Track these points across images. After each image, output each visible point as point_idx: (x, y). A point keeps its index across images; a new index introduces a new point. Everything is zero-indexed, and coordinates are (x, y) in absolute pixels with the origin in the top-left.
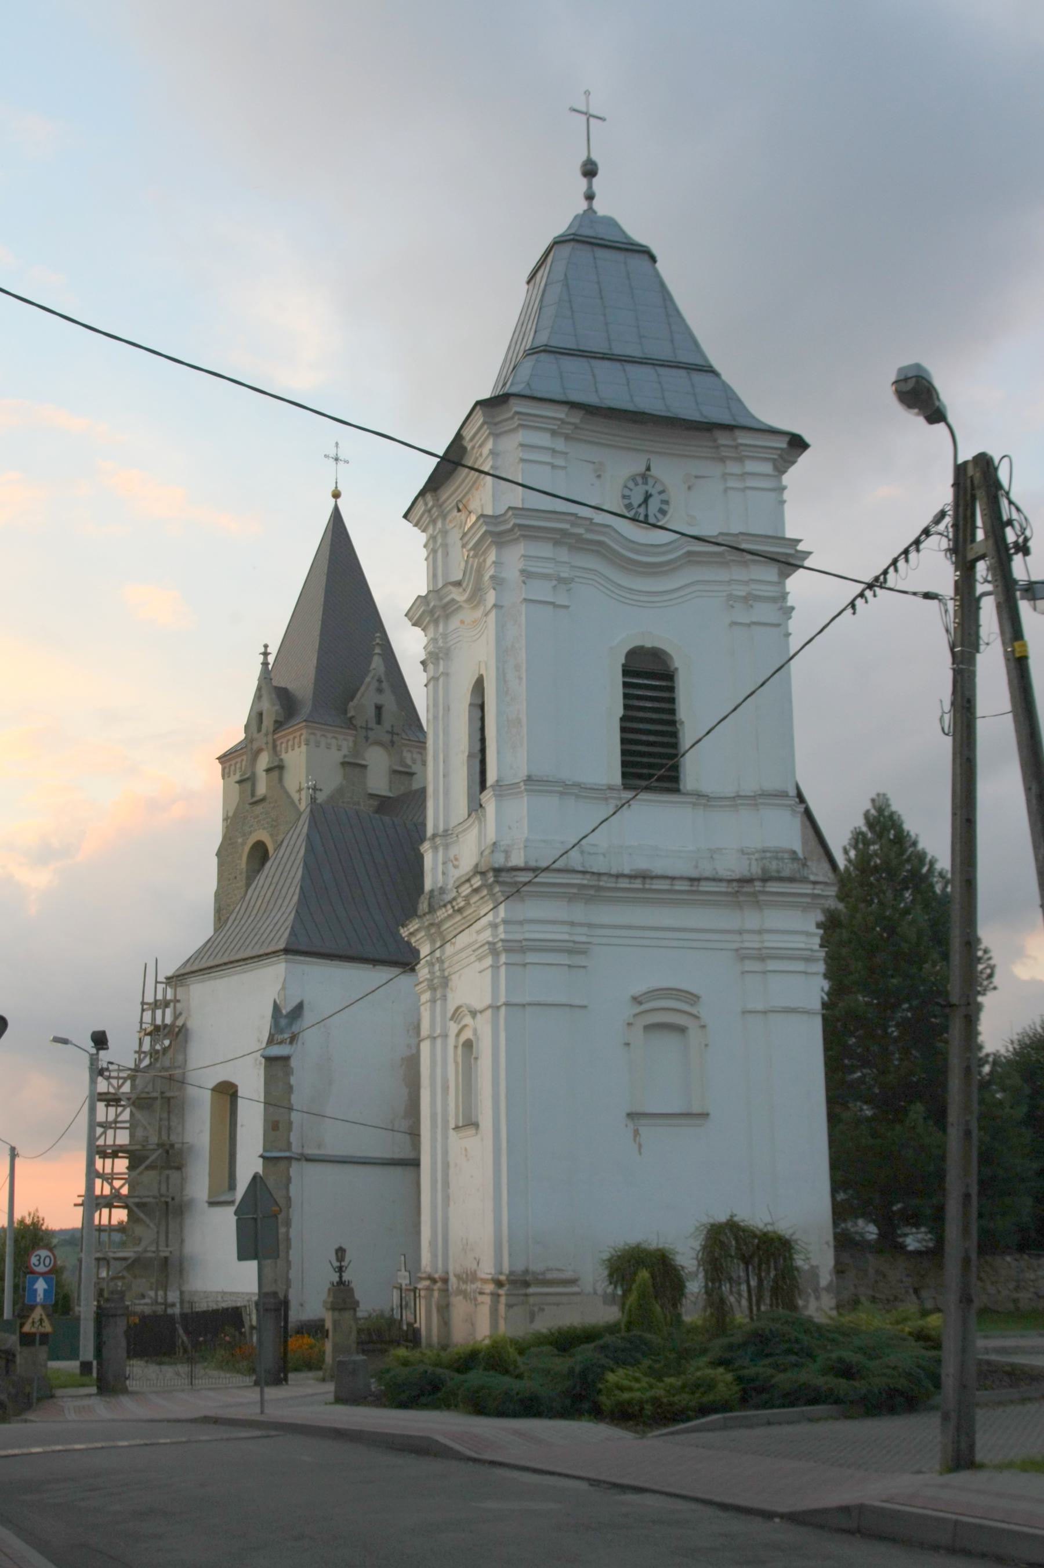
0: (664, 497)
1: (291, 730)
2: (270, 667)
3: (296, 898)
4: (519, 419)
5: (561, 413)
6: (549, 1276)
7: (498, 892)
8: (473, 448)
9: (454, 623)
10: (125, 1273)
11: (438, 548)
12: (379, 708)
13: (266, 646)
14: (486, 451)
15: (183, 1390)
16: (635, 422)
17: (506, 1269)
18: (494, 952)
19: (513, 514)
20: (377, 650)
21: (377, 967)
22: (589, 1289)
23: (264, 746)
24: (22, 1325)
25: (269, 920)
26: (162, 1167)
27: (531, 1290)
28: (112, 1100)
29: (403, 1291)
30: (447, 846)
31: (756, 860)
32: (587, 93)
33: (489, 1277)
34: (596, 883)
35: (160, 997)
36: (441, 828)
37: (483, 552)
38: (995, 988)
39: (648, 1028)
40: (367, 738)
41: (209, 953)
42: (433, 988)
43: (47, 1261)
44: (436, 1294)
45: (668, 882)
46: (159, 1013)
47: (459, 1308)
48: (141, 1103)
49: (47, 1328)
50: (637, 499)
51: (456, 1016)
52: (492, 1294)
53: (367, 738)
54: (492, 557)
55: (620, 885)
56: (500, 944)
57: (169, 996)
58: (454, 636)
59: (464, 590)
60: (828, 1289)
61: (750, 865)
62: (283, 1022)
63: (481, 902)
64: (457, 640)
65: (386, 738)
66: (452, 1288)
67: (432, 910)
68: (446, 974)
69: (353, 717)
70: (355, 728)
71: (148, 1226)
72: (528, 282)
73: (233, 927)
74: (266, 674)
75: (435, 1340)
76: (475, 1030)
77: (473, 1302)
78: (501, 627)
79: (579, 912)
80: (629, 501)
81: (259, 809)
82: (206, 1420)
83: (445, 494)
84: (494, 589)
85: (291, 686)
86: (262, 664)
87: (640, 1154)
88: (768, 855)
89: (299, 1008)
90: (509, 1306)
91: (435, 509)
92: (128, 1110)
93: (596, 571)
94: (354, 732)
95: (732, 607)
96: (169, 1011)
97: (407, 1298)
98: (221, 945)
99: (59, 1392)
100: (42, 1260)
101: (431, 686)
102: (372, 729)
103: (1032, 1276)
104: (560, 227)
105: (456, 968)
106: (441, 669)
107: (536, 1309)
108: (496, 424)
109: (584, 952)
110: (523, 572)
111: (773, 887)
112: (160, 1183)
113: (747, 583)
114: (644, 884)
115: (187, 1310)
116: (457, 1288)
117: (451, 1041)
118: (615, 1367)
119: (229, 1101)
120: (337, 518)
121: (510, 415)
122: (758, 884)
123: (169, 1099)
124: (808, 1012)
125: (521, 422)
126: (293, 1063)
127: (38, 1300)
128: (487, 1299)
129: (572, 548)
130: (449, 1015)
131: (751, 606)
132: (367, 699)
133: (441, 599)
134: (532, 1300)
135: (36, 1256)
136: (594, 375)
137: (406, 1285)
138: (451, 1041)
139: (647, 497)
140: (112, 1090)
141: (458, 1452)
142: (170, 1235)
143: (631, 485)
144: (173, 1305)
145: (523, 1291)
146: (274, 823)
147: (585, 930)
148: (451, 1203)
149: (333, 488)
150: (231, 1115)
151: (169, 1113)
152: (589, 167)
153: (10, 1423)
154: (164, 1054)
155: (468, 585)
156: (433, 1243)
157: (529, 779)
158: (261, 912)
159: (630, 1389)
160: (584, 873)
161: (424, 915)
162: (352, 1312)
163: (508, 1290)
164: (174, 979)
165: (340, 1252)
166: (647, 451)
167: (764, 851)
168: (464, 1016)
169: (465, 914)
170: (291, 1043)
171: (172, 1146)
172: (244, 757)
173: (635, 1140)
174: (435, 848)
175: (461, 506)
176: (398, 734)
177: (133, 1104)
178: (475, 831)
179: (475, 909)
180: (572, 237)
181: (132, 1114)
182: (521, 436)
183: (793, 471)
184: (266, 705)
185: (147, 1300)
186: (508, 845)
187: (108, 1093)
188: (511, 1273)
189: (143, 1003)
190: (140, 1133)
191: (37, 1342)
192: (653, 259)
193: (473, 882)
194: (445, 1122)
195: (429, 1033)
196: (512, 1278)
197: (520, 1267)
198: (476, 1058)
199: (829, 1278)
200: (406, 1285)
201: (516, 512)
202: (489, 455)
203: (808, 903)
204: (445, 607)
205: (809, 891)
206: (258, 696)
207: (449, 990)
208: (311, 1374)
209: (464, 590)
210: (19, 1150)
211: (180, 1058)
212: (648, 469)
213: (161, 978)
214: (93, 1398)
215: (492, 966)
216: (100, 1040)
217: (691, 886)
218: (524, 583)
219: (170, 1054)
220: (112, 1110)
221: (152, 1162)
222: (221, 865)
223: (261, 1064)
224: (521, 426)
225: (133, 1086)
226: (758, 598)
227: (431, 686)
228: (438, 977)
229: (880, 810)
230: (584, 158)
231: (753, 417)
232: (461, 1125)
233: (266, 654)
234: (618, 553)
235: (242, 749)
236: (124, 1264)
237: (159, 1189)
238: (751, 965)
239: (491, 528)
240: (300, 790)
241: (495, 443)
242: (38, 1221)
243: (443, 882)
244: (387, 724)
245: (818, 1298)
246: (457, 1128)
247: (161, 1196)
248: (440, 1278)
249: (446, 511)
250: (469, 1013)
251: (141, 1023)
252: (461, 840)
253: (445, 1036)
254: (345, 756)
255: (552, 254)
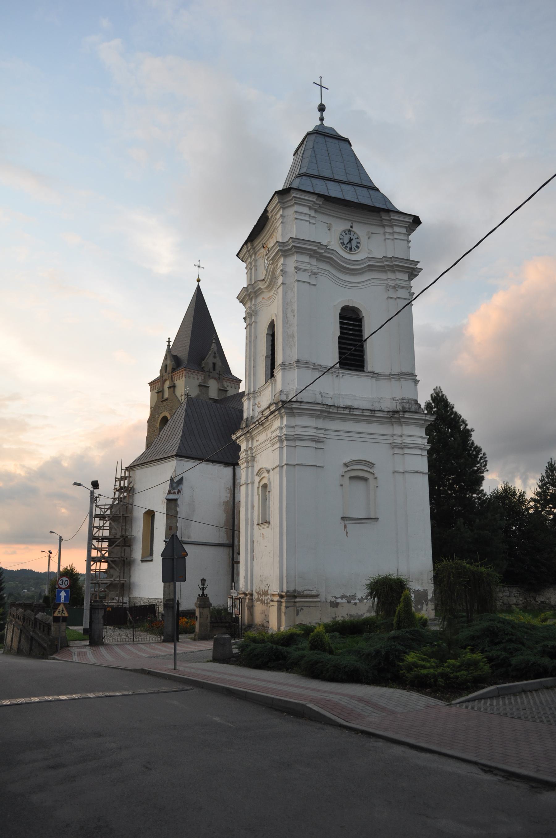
0: (358, 240)
1: (179, 371)
2: (171, 347)
3: (181, 434)
4: (295, 200)
5: (313, 198)
6: (305, 593)
7: (283, 412)
8: (272, 217)
9: (260, 299)
10: (106, 589)
11: (253, 267)
12: (214, 364)
13: (169, 339)
14: (278, 216)
15: (129, 644)
16: (346, 206)
17: (285, 589)
18: (281, 441)
19: (292, 241)
20: (214, 341)
21: (214, 464)
22: (324, 600)
23: (168, 378)
24: (54, 612)
25: (169, 443)
26: (123, 546)
27: (297, 600)
28: (101, 517)
29: (233, 600)
30: (255, 398)
31: (399, 403)
32: (321, 77)
33: (277, 593)
34: (328, 410)
35: (123, 475)
36: (252, 390)
37: (276, 262)
38: (487, 471)
39: (351, 478)
40: (209, 376)
41: (144, 458)
42: (247, 462)
43: (66, 583)
44: (247, 601)
45: (361, 411)
46: (122, 482)
47: (259, 608)
48: (114, 519)
49: (66, 614)
50: (346, 240)
51: (259, 473)
52: (278, 601)
53: (209, 376)
54: (281, 261)
55: (339, 412)
56: (284, 436)
57: (127, 475)
58: (259, 305)
59: (266, 282)
60: (431, 600)
61: (397, 405)
62: (175, 485)
63: (274, 418)
64: (261, 307)
65: (217, 376)
66: (255, 598)
67: (247, 426)
68: (254, 455)
69: (204, 367)
70: (204, 371)
71: (116, 570)
72: (294, 155)
73: (155, 446)
74: (169, 350)
75: (246, 621)
76: (269, 479)
77: (266, 605)
78: (285, 293)
79: (320, 423)
80: (343, 241)
81: (165, 403)
82: (143, 671)
83: (256, 243)
84: (282, 276)
85: (179, 355)
86: (167, 346)
87: (347, 536)
88: (405, 401)
89: (181, 480)
90: (287, 607)
91: (251, 250)
92: (108, 522)
93: (328, 271)
94: (204, 373)
95: (389, 290)
96: (126, 481)
97: (236, 603)
98: (149, 454)
99: (71, 643)
100: (64, 582)
101: (248, 328)
102: (211, 372)
103: (501, 596)
104: (311, 129)
105: (259, 451)
106: (253, 320)
107: (299, 609)
108: (283, 203)
109: (322, 442)
110: (296, 267)
111: (407, 415)
112: (121, 552)
113: (395, 280)
114: (350, 411)
115: (132, 605)
116: (258, 598)
117: (256, 485)
118: (407, 651)
119: (151, 518)
120: (198, 290)
121: (290, 198)
122: (401, 414)
123: (126, 517)
124: (423, 473)
125: (295, 201)
126: (179, 502)
127: (62, 601)
128: (276, 604)
129: (318, 260)
130: (255, 473)
131: (397, 290)
132: (209, 360)
133: (254, 289)
134: (297, 604)
135: (61, 580)
136: (327, 187)
137: (235, 596)
138: (256, 485)
139: (351, 240)
140: (102, 513)
141: (330, 719)
142: (125, 574)
143: (344, 234)
144: (126, 603)
145: (293, 600)
146: (171, 409)
147: (323, 432)
148: (255, 559)
149: (197, 278)
150: (151, 527)
151: (126, 523)
152: (322, 107)
153: (47, 659)
154: (124, 499)
155: (267, 280)
156: (245, 578)
157: (298, 361)
158: (166, 440)
159: (424, 667)
160: (323, 404)
161: (244, 428)
162: (208, 608)
163: (286, 600)
164: (129, 468)
165: (203, 581)
166: (351, 220)
167: (403, 399)
168: (264, 472)
169: (264, 426)
170: (178, 494)
171: (127, 537)
172: (159, 383)
173: (345, 530)
174: (249, 399)
175: (265, 246)
176: (221, 375)
177: (111, 519)
178: (269, 389)
179: (270, 422)
180: (316, 131)
181: (110, 523)
182: (296, 208)
183: (414, 234)
184: (169, 362)
185: (115, 601)
186: (288, 392)
187: (101, 514)
188: (288, 591)
189: (116, 478)
190: (113, 531)
191: (61, 621)
192: (350, 145)
193: (271, 408)
194: (253, 523)
195: (245, 482)
196: (288, 594)
197: (292, 589)
198: (269, 492)
199: (432, 595)
200: (235, 596)
201: (294, 240)
202: (280, 217)
203: (423, 423)
204: (255, 292)
205: (424, 418)
206: (166, 358)
207: (255, 462)
208: (187, 636)
209: (266, 282)
210: (63, 538)
211: (131, 500)
212: (352, 227)
213: (124, 468)
214: (87, 647)
215: (279, 447)
216: (95, 485)
217: (371, 413)
218: (296, 273)
219: (127, 499)
220: (102, 522)
221: (118, 543)
222: (149, 426)
223: (165, 503)
224: (295, 203)
225: (111, 512)
226: (400, 287)
227: (248, 328)
228: (250, 456)
229: (437, 394)
230: (320, 103)
231: (397, 209)
232: (260, 523)
233: (169, 342)
234: (338, 263)
235: (158, 379)
236: (106, 585)
237: (121, 555)
238: (397, 451)
239: (281, 248)
240: (182, 396)
241: (283, 212)
242: (73, 568)
243: (253, 414)
244: (217, 371)
245: (427, 605)
246: (258, 524)
247: (122, 557)
248: (249, 593)
249: (256, 251)
250: (266, 471)
251: (115, 486)
252: (262, 394)
253: (253, 483)
254: (200, 383)
255: (307, 139)
